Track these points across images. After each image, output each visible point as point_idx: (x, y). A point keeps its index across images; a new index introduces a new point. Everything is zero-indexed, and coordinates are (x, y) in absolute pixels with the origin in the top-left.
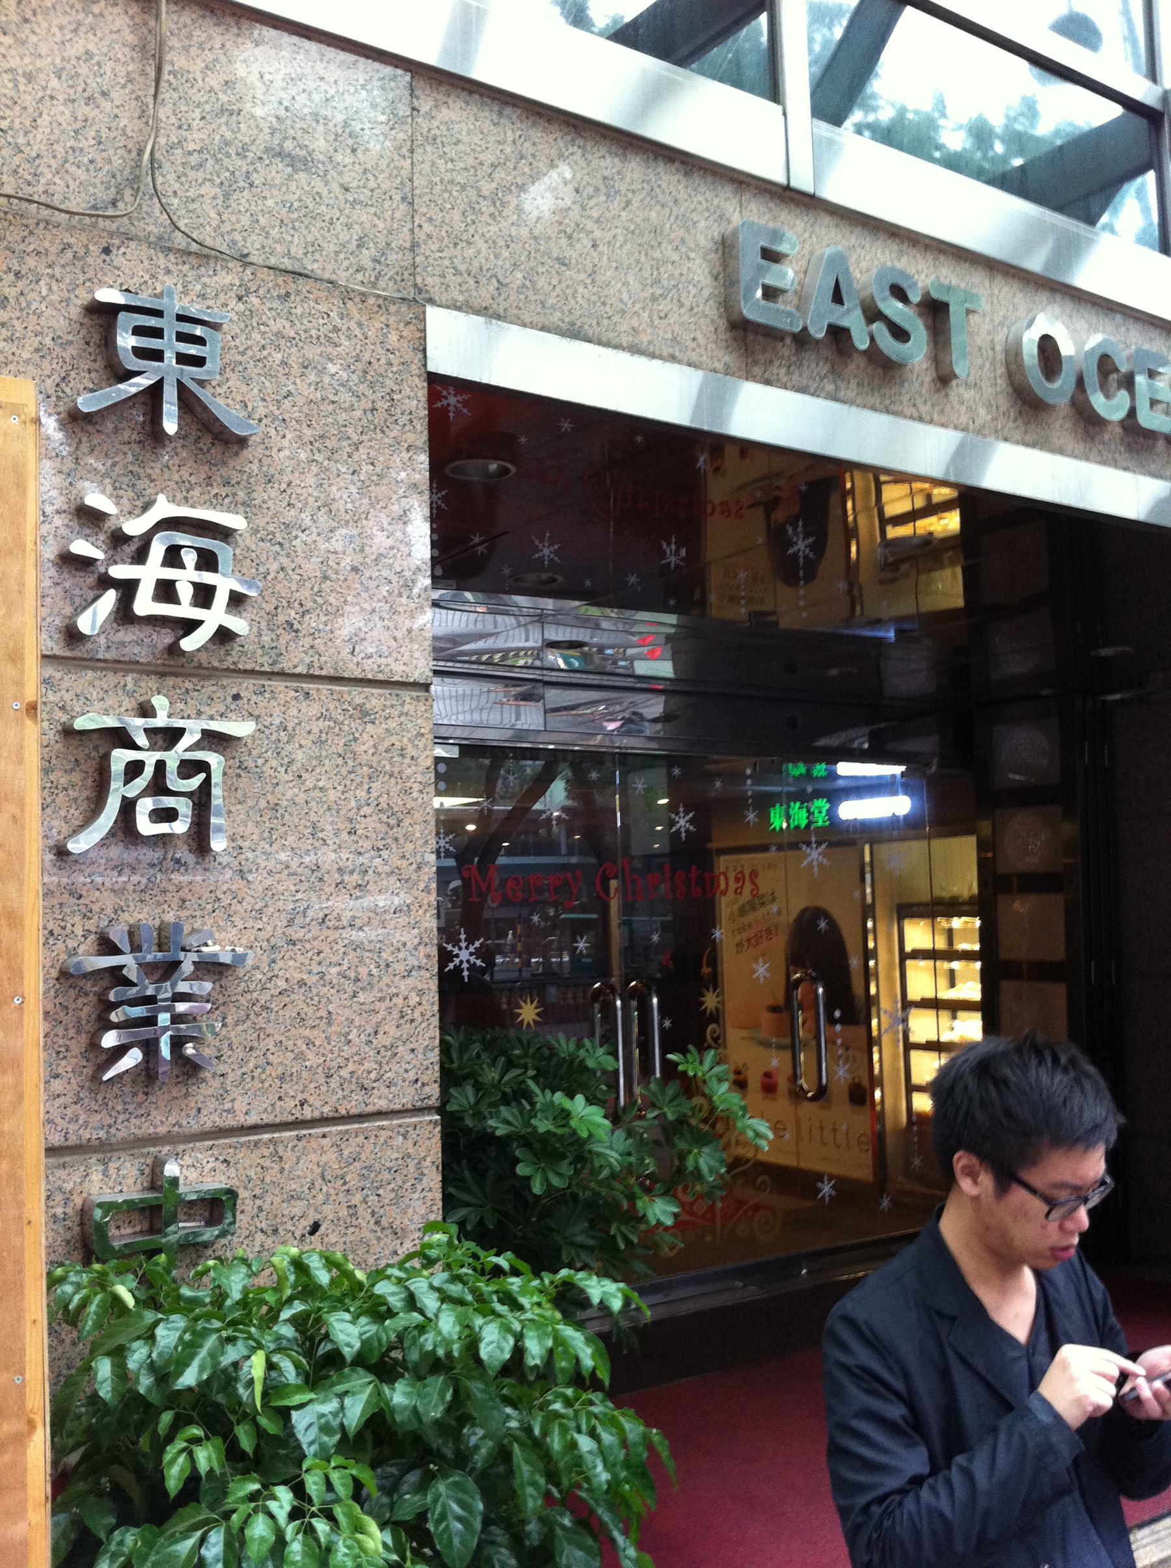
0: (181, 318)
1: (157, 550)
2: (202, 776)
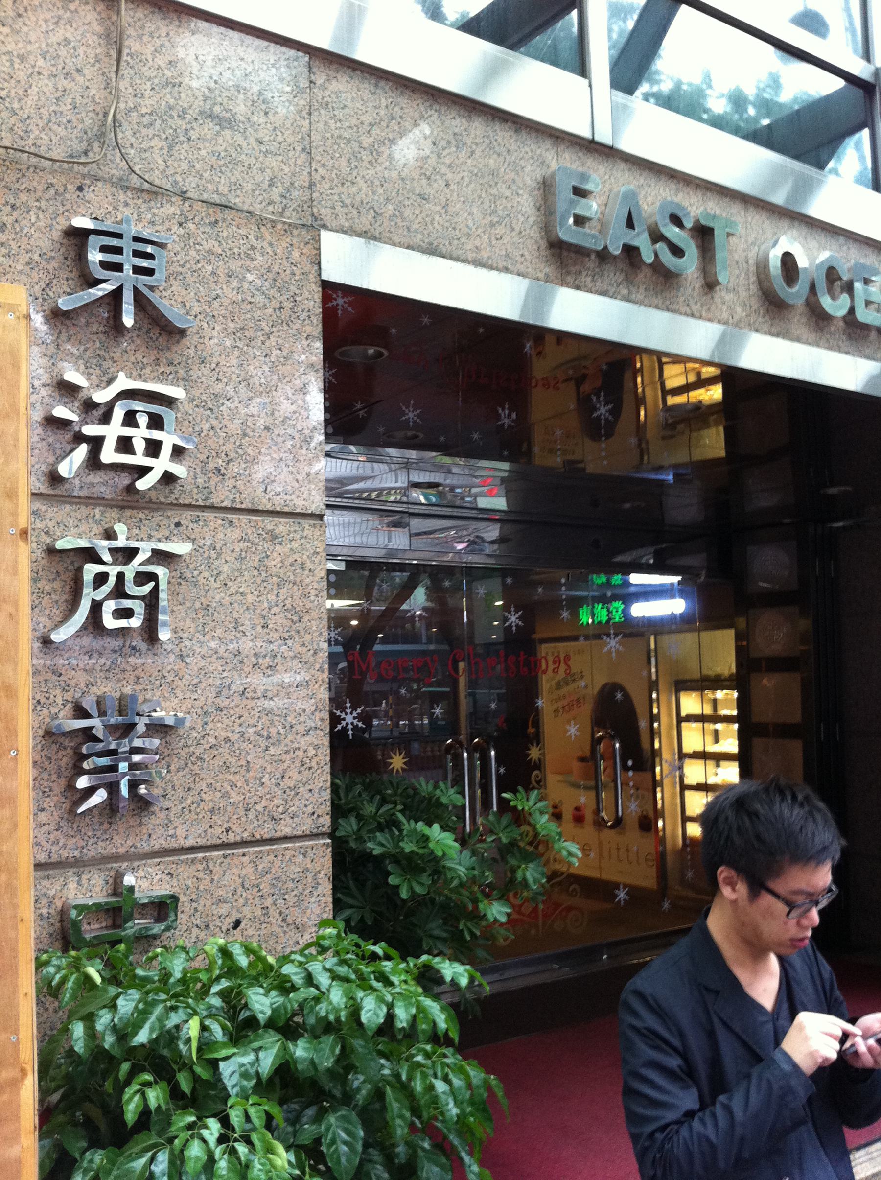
0: (136, 239)
1: (118, 414)
2: (152, 584)
